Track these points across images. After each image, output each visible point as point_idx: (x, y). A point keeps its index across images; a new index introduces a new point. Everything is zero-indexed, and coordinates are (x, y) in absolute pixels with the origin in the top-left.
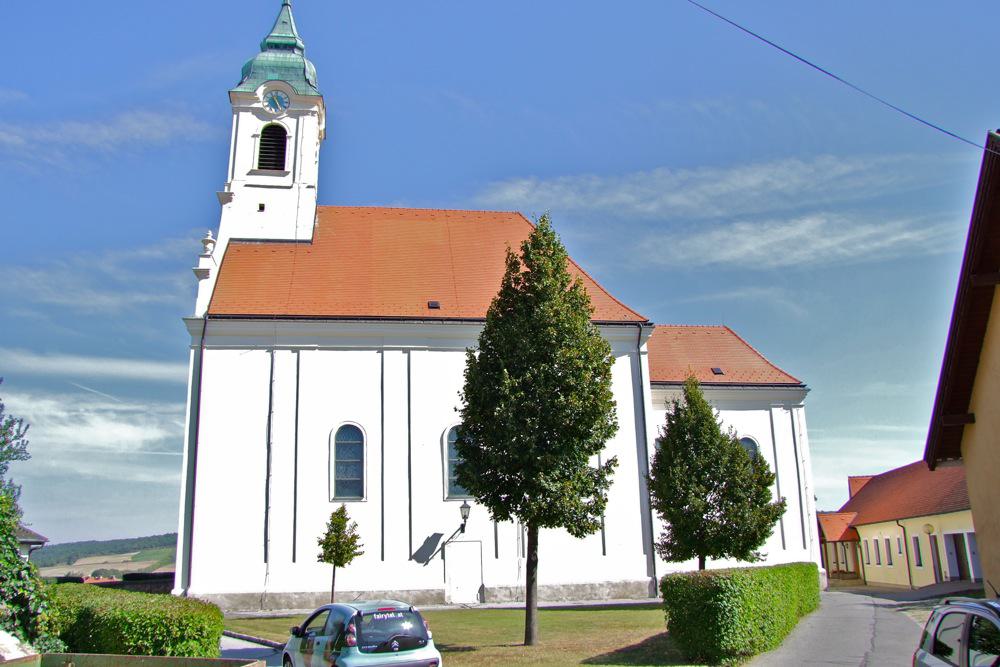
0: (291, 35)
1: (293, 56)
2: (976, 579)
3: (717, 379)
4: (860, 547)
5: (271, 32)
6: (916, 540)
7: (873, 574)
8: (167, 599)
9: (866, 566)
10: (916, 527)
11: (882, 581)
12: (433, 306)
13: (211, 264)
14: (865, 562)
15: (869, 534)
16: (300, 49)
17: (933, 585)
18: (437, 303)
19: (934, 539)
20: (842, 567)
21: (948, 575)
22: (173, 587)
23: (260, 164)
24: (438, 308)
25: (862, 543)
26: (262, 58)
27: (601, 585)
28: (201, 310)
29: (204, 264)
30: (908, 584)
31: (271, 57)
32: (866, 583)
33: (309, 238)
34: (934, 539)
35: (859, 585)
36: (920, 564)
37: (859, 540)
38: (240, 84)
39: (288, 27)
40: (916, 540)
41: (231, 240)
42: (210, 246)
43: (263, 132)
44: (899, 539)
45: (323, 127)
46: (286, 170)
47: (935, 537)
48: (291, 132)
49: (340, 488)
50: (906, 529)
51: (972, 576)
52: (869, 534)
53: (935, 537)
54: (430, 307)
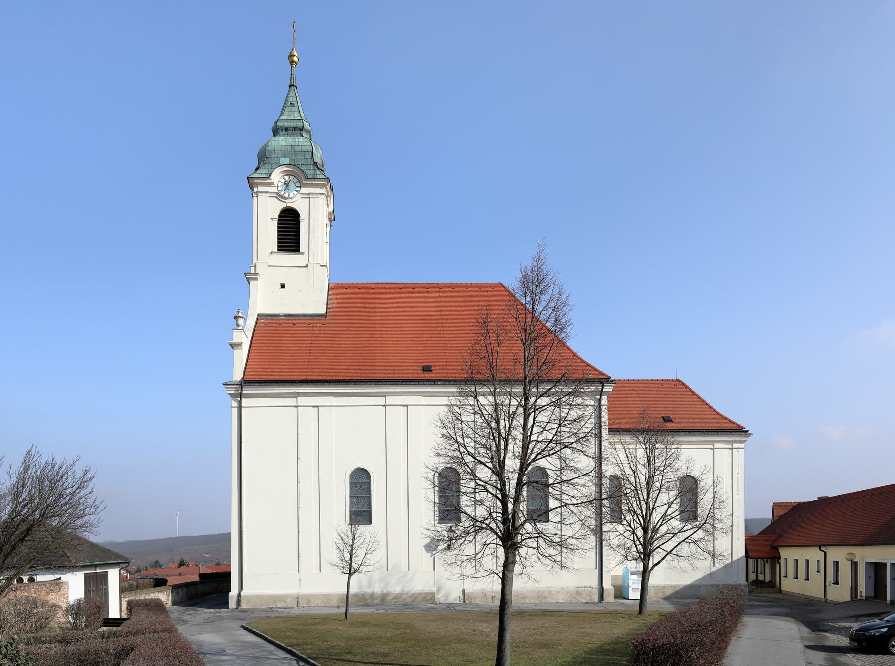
0: (300, 118)
1: (301, 139)
2: (891, 601)
3: (427, 375)
4: (779, 563)
5: (282, 114)
6: (836, 563)
7: (789, 585)
8: (223, 612)
9: (782, 578)
10: (838, 554)
11: (797, 592)
12: (427, 369)
13: (244, 338)
14: (782, 575)
15: (788, 554)
16: (308, 132)
17: (849, 601)
18: (430, 366)
19: (854, 565)
20: (761, 578)
21: (864, 595)
22: (229, 590)
23: (279, 246)
24: (431, 371)
25: (782, 561)
26: (274, 143)
27: (558, 592)
28: (238, 376)
29: (237, 337)
30: (823, 597)
31: (282, 141)
32: (780, 591)
33: (324, 312)
34: (854, 565)
35: (776, 593)
36: (837, 583)
37: (779, 558)
38: (256, 169)
39: (295, 109)
40: (836, 563)
41: (259, 315)
42: (241, 321)
43: (280, 216)
44: (819, 561)
45: (331, 209)
46: (302, 250)
47: (856, 563)
48: (303, 216)
49: (353, 517)
50: (828, 555)
51: (888, 598)
52: (788, 554)
53: (856, 563)
54: (423, 371)
